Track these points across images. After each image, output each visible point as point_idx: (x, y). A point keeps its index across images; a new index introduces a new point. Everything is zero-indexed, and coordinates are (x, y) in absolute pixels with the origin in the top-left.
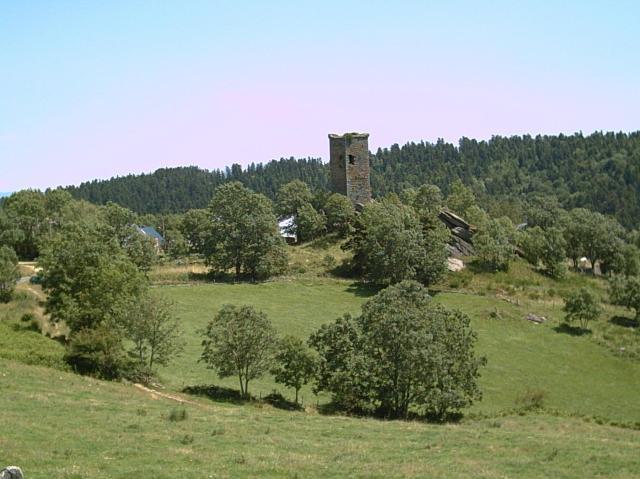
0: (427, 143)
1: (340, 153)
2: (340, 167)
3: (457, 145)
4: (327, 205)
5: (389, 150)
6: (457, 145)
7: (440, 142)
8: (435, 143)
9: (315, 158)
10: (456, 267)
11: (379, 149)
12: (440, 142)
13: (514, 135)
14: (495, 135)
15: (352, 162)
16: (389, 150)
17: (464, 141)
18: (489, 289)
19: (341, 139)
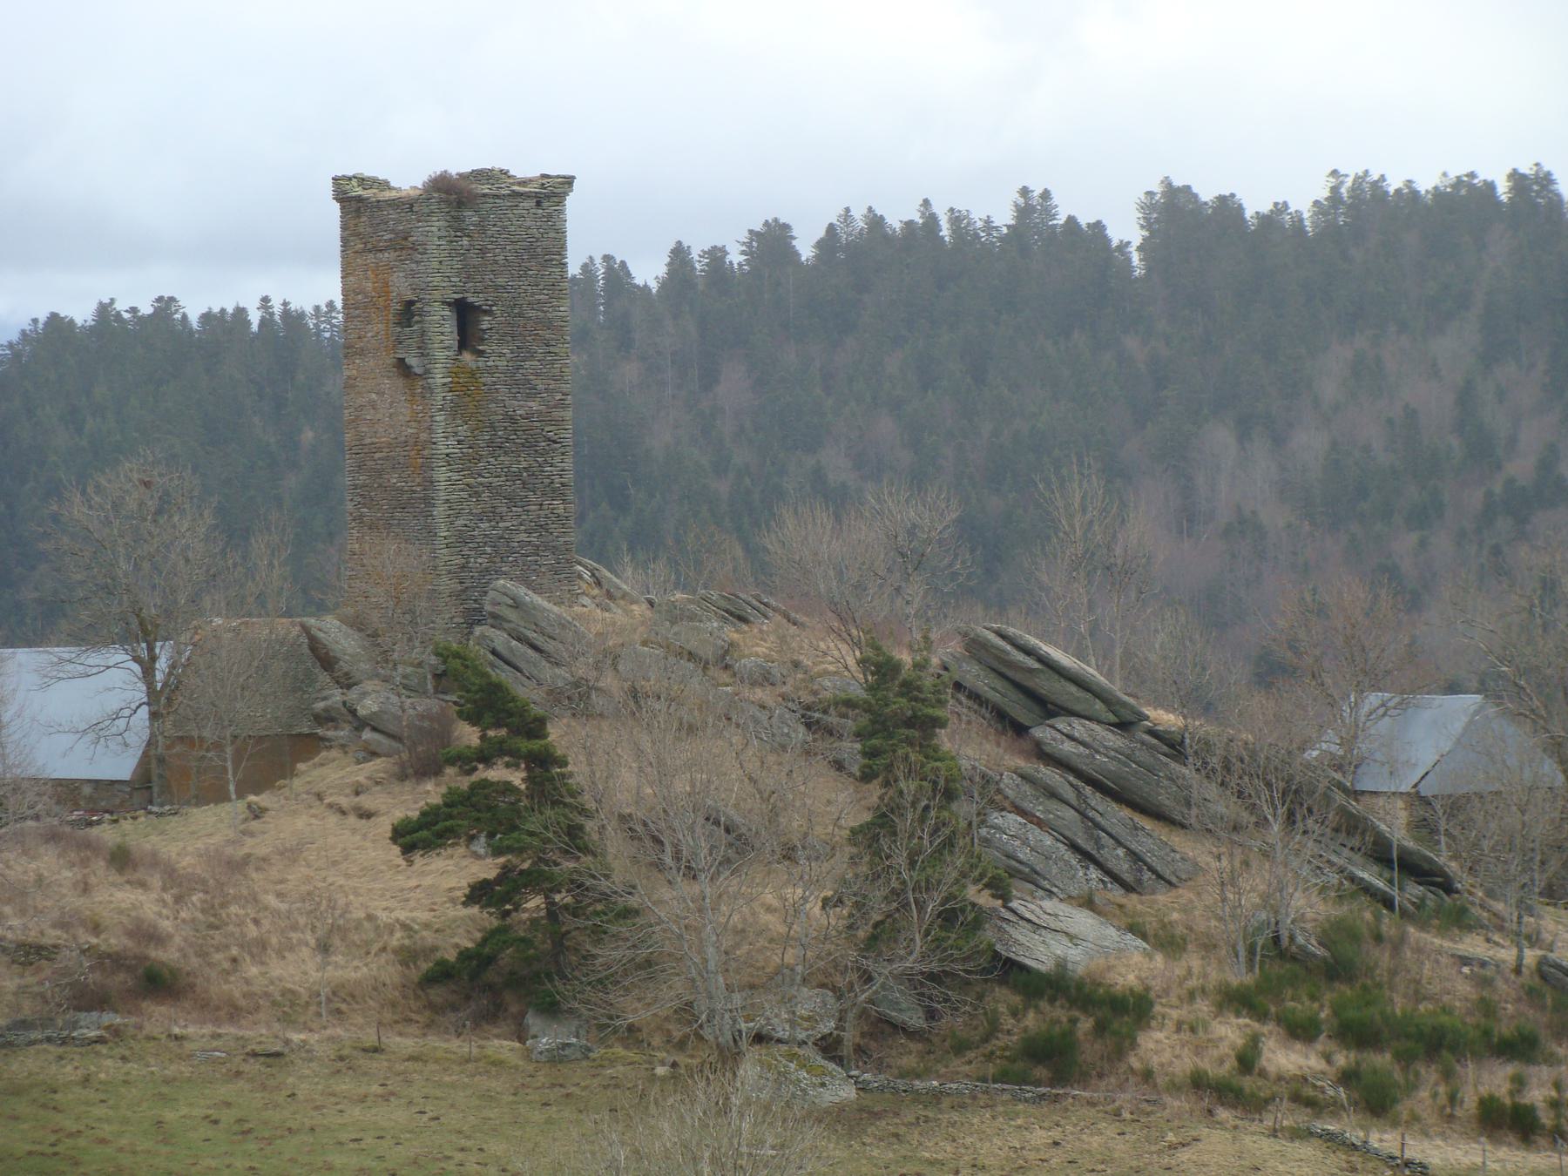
0: (956, 219)
1: (401, 286)
2: (403, 368)
3: (1126, 230)
4: (508, 996)
5: (735, 257)
6: (1126, 230)
7: (1033, 208)
8: (1004, 217)
9: (205, 310)
10: (1060, 948)
11: (1025, 192)
12: (1033, 208)
13: (1457, 170)
14: (1351, 170)
15: (467, 337)
16: (735, 257)
17: (1173, 212)
18: (375, 635)
19: (407, 205)
